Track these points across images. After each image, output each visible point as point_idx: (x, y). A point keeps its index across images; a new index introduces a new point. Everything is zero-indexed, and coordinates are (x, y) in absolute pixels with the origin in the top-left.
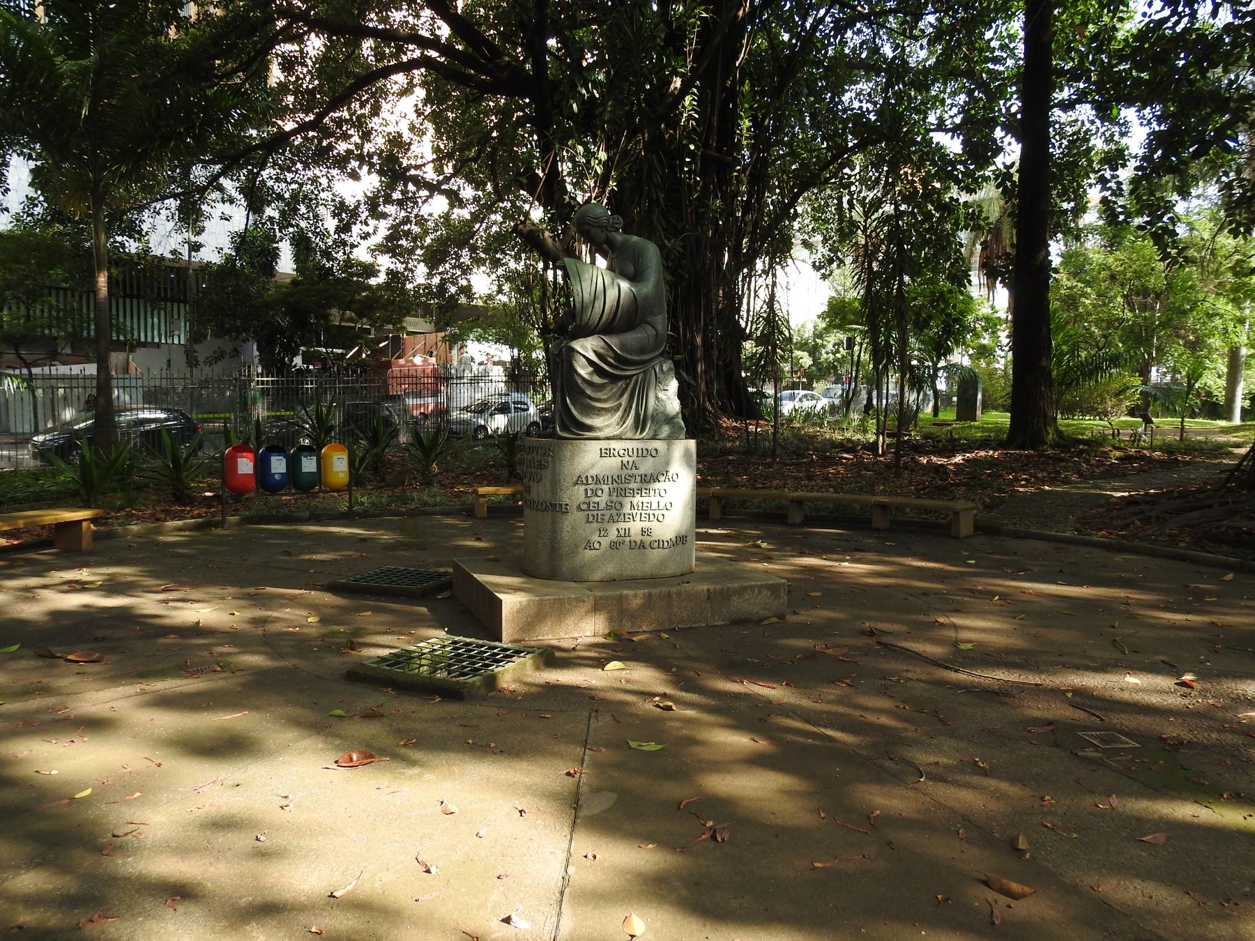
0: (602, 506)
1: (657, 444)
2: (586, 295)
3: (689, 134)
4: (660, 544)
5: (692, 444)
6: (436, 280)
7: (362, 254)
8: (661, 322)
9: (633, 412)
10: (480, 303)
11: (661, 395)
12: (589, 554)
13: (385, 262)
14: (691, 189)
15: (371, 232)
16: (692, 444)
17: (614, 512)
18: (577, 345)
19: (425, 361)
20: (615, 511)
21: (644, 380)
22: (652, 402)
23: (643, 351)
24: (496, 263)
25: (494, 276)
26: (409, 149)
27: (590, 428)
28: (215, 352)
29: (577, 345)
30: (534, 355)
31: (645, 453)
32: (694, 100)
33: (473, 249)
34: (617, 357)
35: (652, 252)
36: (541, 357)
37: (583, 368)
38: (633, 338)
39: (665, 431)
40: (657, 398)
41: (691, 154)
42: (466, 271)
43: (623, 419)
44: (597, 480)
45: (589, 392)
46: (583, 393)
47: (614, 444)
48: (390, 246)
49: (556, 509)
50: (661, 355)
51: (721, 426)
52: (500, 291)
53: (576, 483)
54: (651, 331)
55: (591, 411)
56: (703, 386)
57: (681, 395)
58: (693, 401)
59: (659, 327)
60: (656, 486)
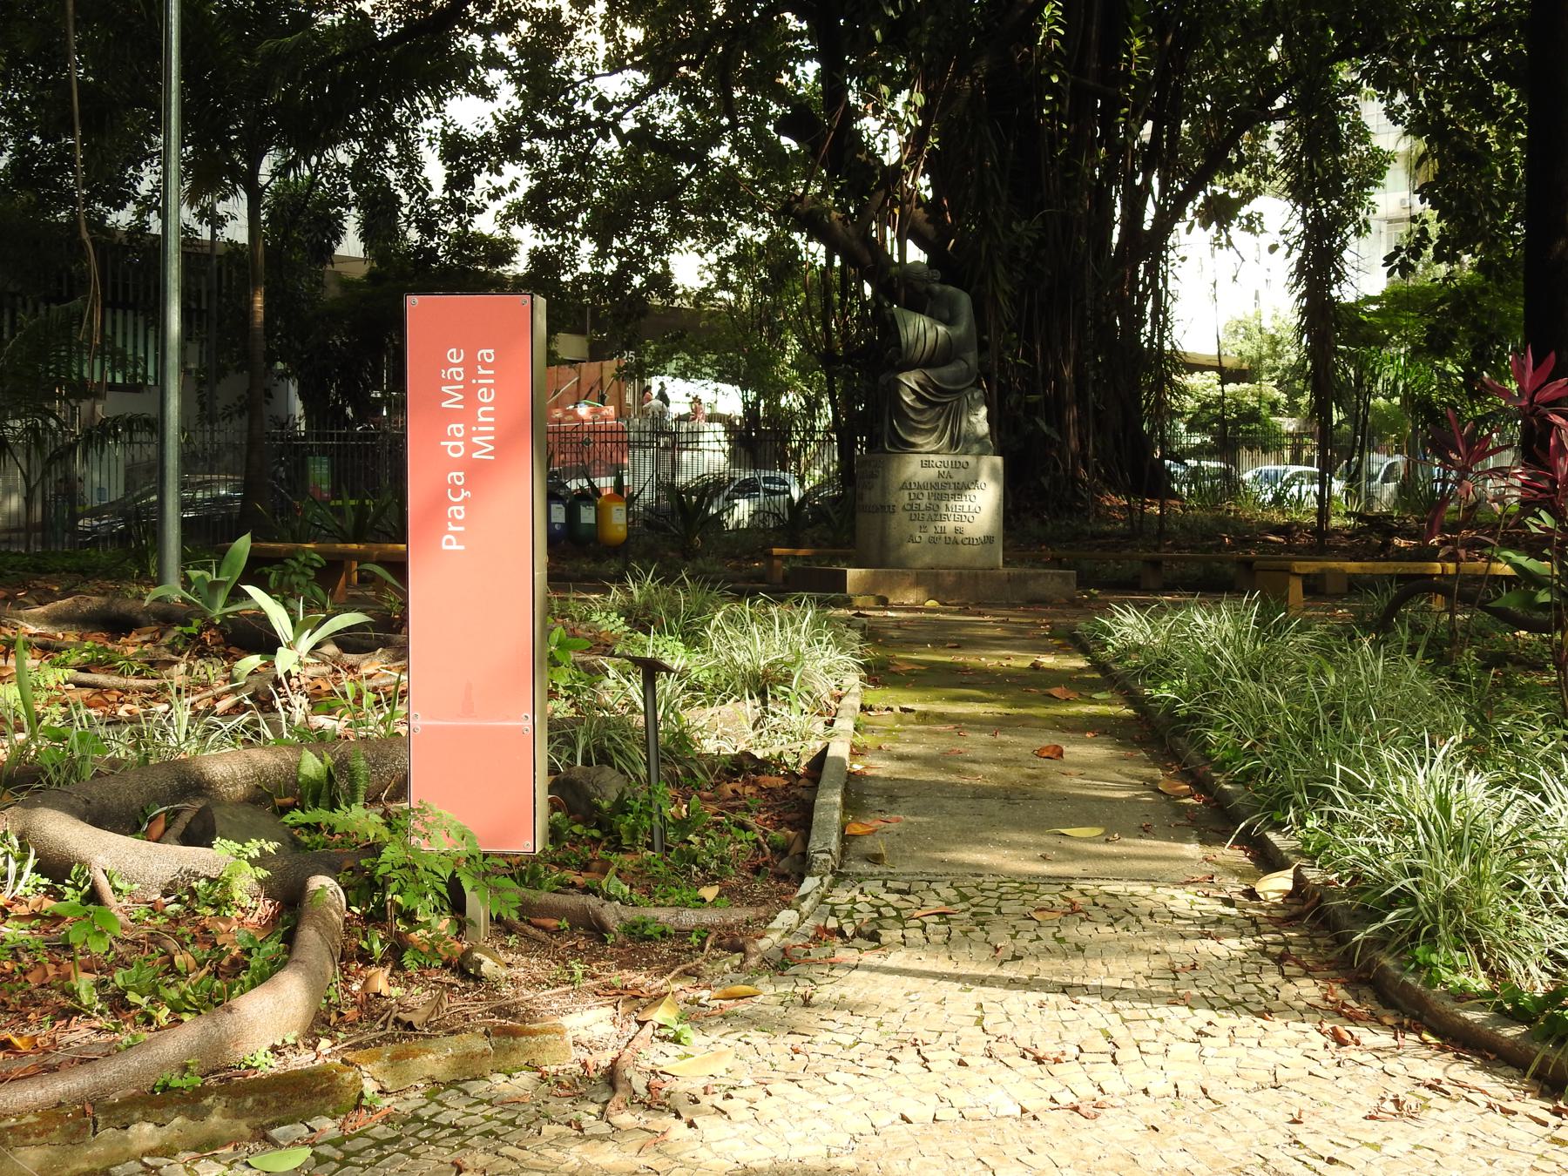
0: (923, 507)
1: (968, 458)
2: (910, 338)
3: (1051, 59)
4: (970, 541)
5: (999, 460)
6: (611, 267)
7: (485, 224)
8: (972, 357)
9: (948, 432)
10: (686, 304)
11: (973, 419)
12: (911, 545)
13: (528, 238)
14: (1054, 142)
15: (506, 186)
16: (999, 460)
17: (932, 513)
18: (903, 378)
19: (595, 411)
20: (935, 514)
21: (958, 405)
22: (964, 424)
23: (956, 382)
24: (719, 233)
25: (712, 258)
26: (571, 37)
27: (913, 445)
28: (239, 398)
29: (903, 378)
30: (783, 402)
31: (956, 466)
32: (1057, 7)
33: (675, 209)
34: (936, 387)
35: (964, 299)
36: (796, 406)
37: (908, 396)
38: (948, 371)
39: (976, 448)
40: (969, 421)
41: (1053, 89)
42: (661, 245)
43: (940, 438)
44: (919, 487)
45: (912, 415)
46: (907, 416)
47: (932, 457)
48: (535, 209)
49: (885, 509)
50: (972, 386)
51: (1100, 505)
52: (723, 284)
53: (902, 488)
54: (964, 366)
55: (914, 431)
56: (1074, 444)
57: (989, 418)
58: (1056, 467)
59: (971, 362)
60: (968, 493)
